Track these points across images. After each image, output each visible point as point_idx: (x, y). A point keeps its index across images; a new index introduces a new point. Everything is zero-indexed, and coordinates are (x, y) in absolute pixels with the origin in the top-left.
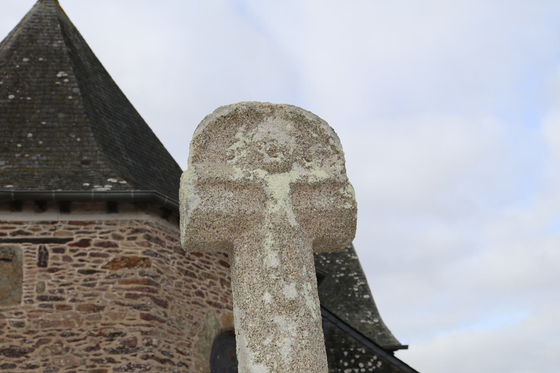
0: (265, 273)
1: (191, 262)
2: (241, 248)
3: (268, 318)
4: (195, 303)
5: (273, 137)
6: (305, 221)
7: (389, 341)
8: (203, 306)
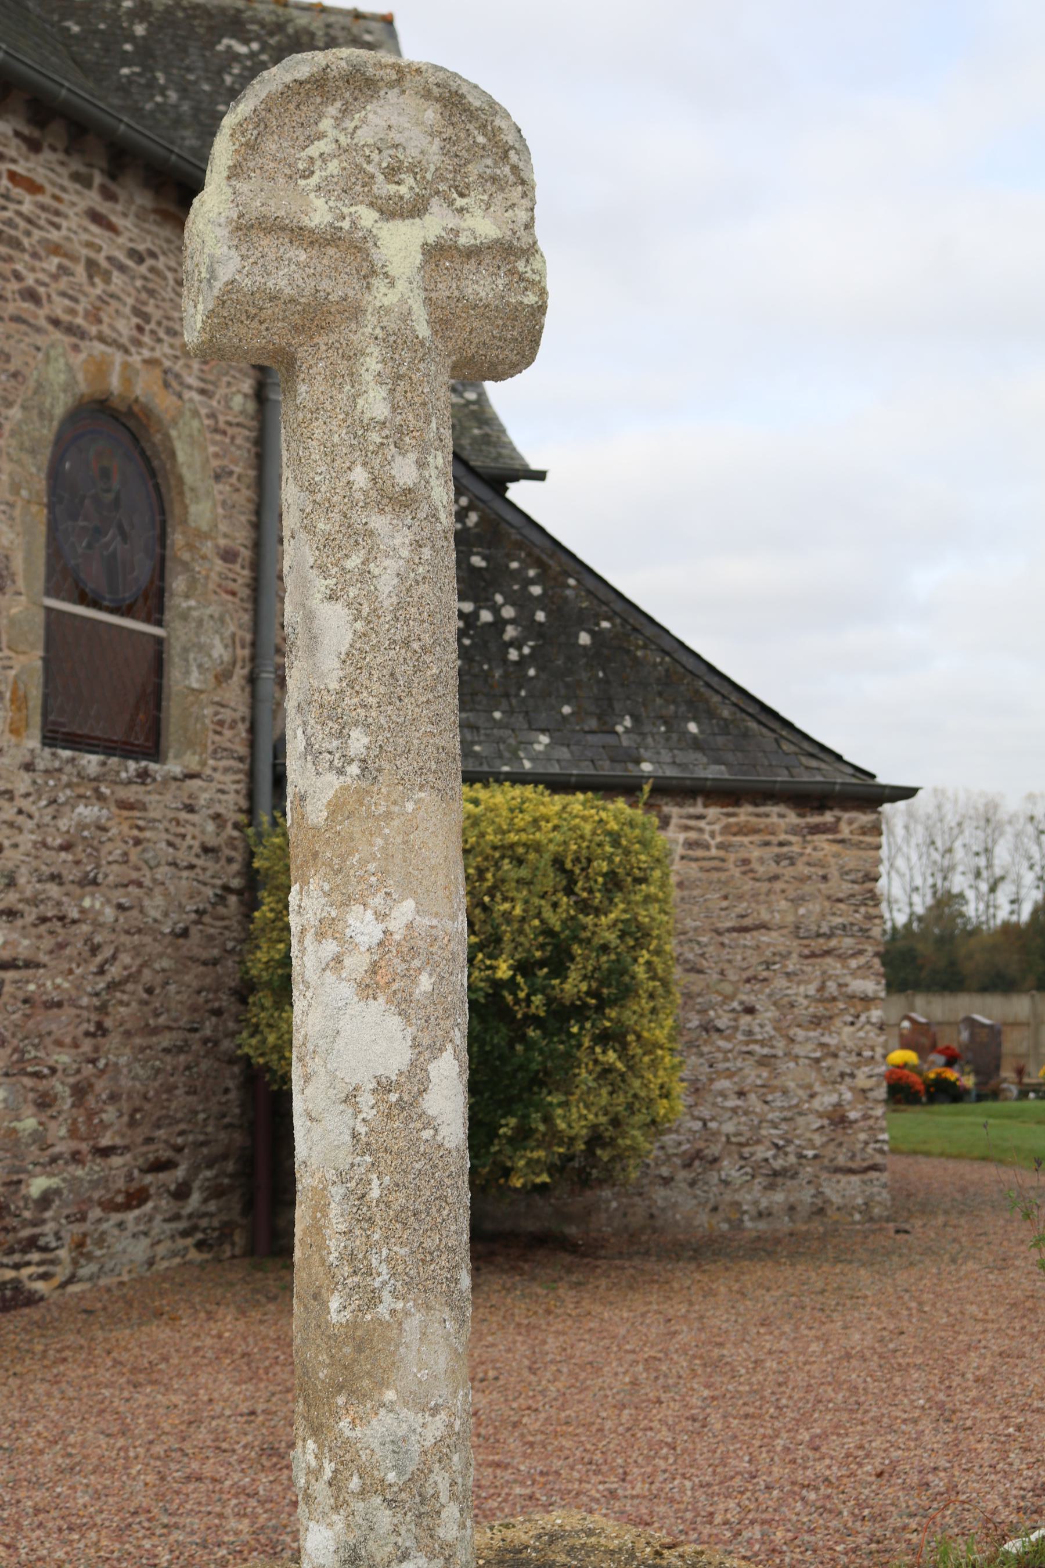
0: (359, 427)
1: (13, 206)
2: (310, 367)
3: (358, 517)
4: (17, 319)
5: (398, 138)
6: (441, 323)
7: (500, 455)
8: (38, 330)
